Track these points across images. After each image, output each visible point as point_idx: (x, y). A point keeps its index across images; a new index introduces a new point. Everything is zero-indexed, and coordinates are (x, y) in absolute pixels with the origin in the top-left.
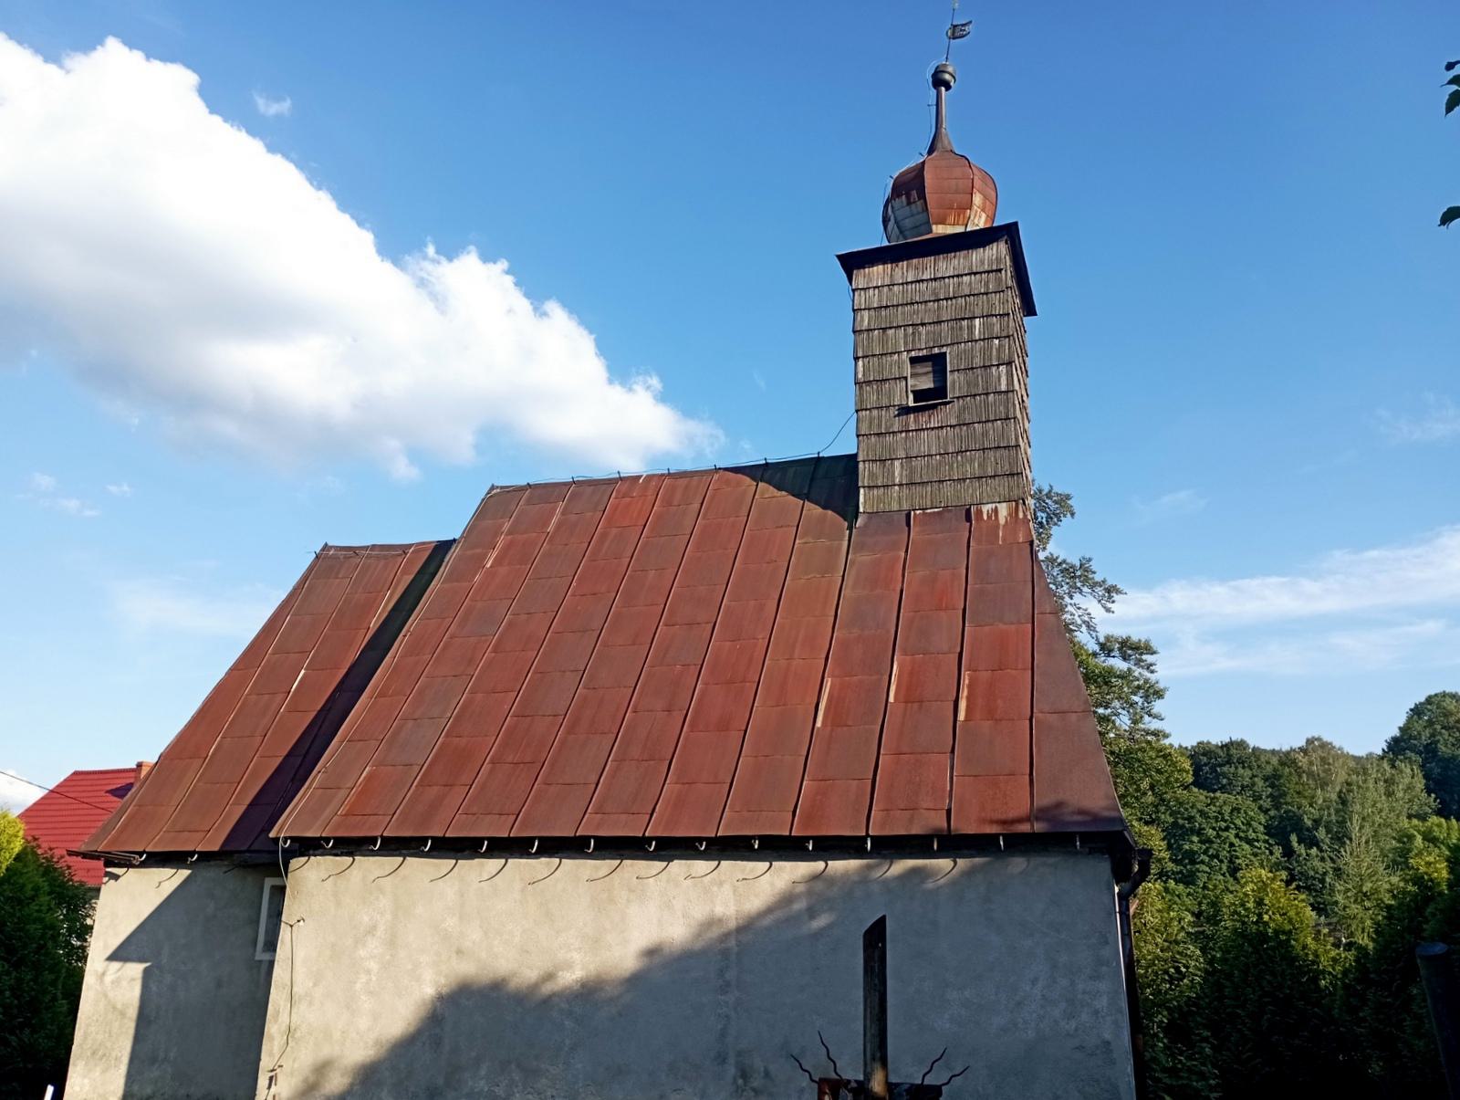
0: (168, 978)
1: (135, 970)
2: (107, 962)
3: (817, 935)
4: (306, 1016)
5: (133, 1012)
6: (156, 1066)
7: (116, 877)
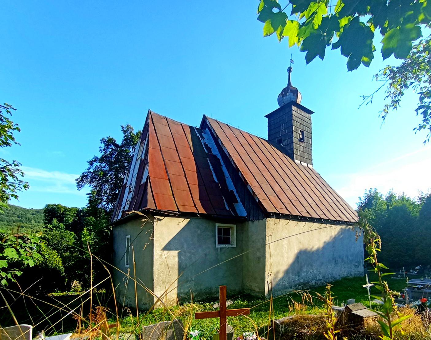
0: (188, 255)
1: (175, 253)
2: (162, 251)
3: (342, 238)
4: (274, 259)
5: (176, 267)
6: (189, 282)
7: (160, 220)
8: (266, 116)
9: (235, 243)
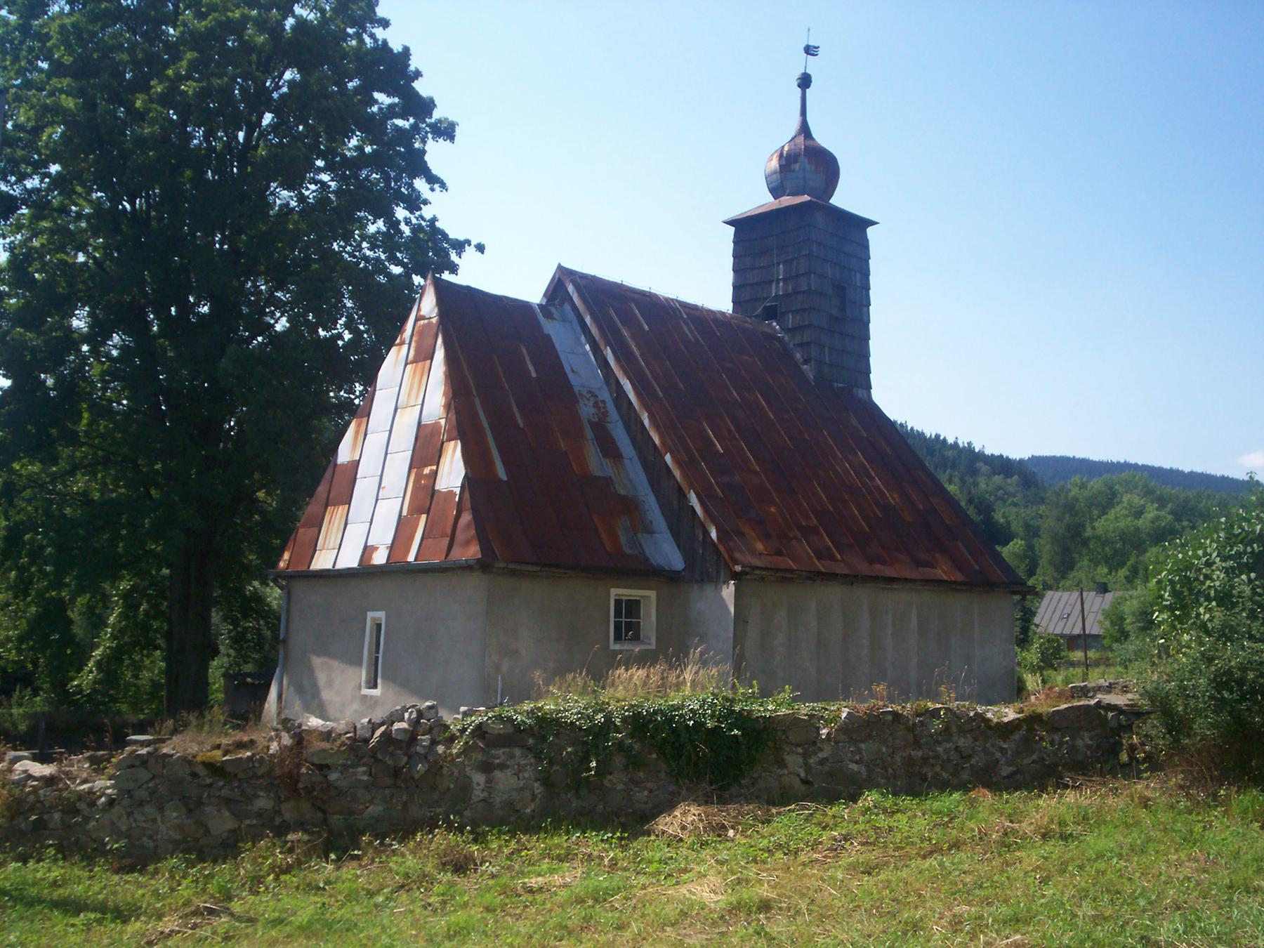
8: (730, 223)
9: (653, 640)
